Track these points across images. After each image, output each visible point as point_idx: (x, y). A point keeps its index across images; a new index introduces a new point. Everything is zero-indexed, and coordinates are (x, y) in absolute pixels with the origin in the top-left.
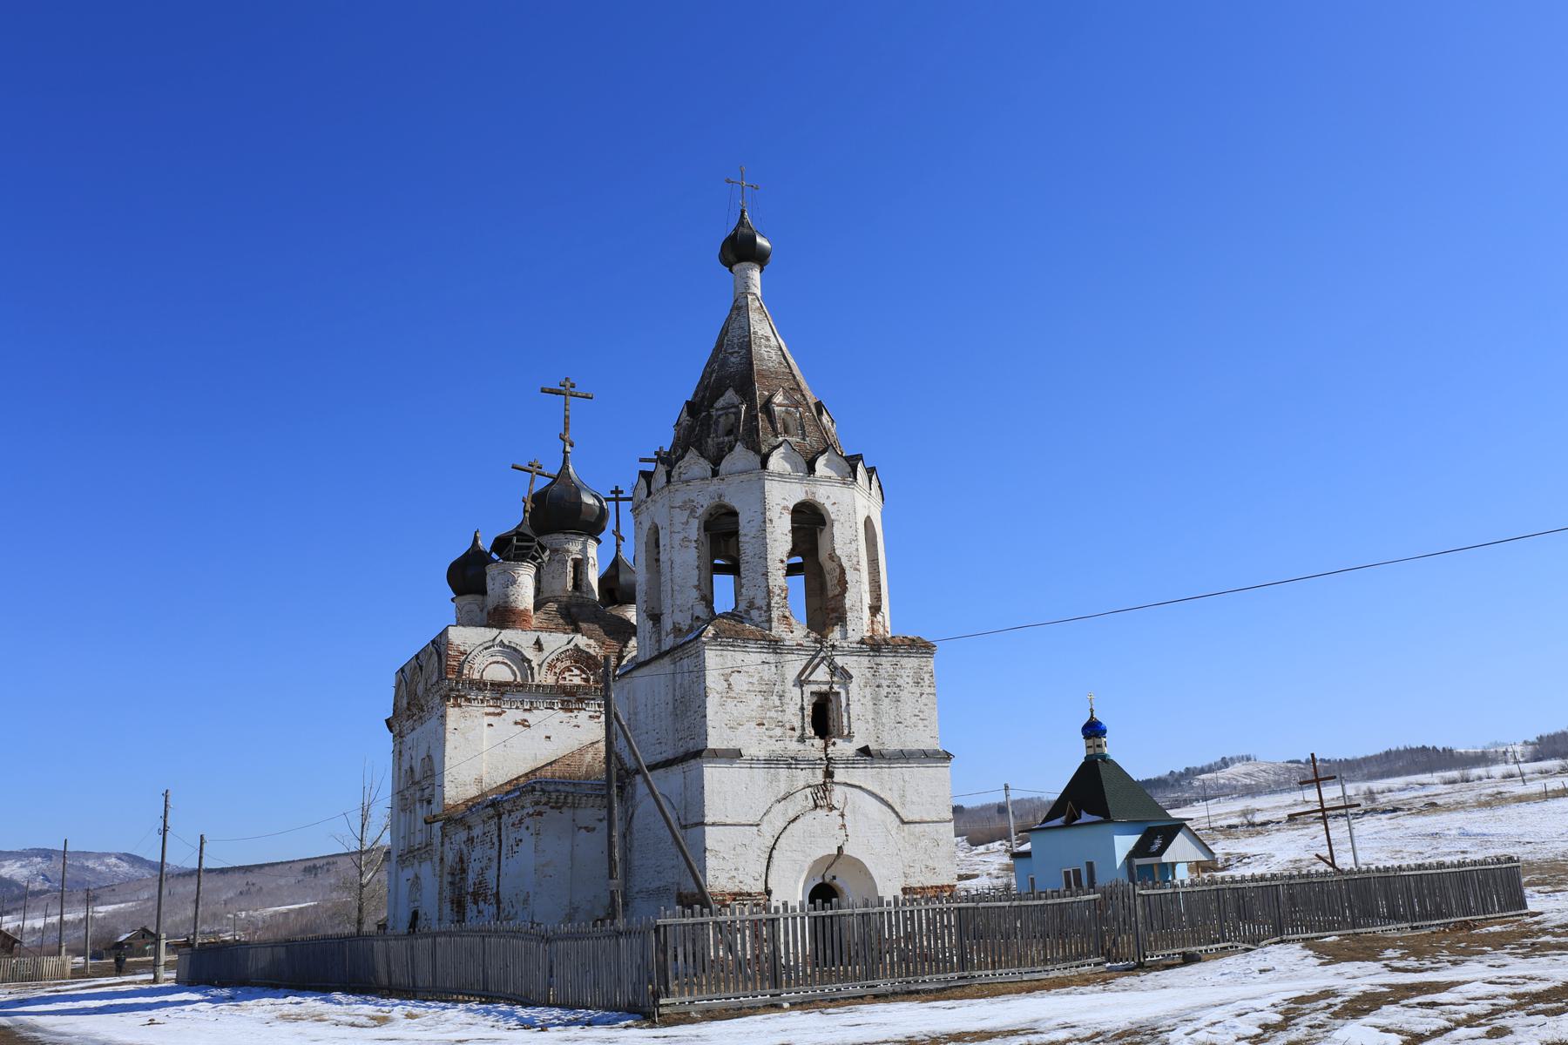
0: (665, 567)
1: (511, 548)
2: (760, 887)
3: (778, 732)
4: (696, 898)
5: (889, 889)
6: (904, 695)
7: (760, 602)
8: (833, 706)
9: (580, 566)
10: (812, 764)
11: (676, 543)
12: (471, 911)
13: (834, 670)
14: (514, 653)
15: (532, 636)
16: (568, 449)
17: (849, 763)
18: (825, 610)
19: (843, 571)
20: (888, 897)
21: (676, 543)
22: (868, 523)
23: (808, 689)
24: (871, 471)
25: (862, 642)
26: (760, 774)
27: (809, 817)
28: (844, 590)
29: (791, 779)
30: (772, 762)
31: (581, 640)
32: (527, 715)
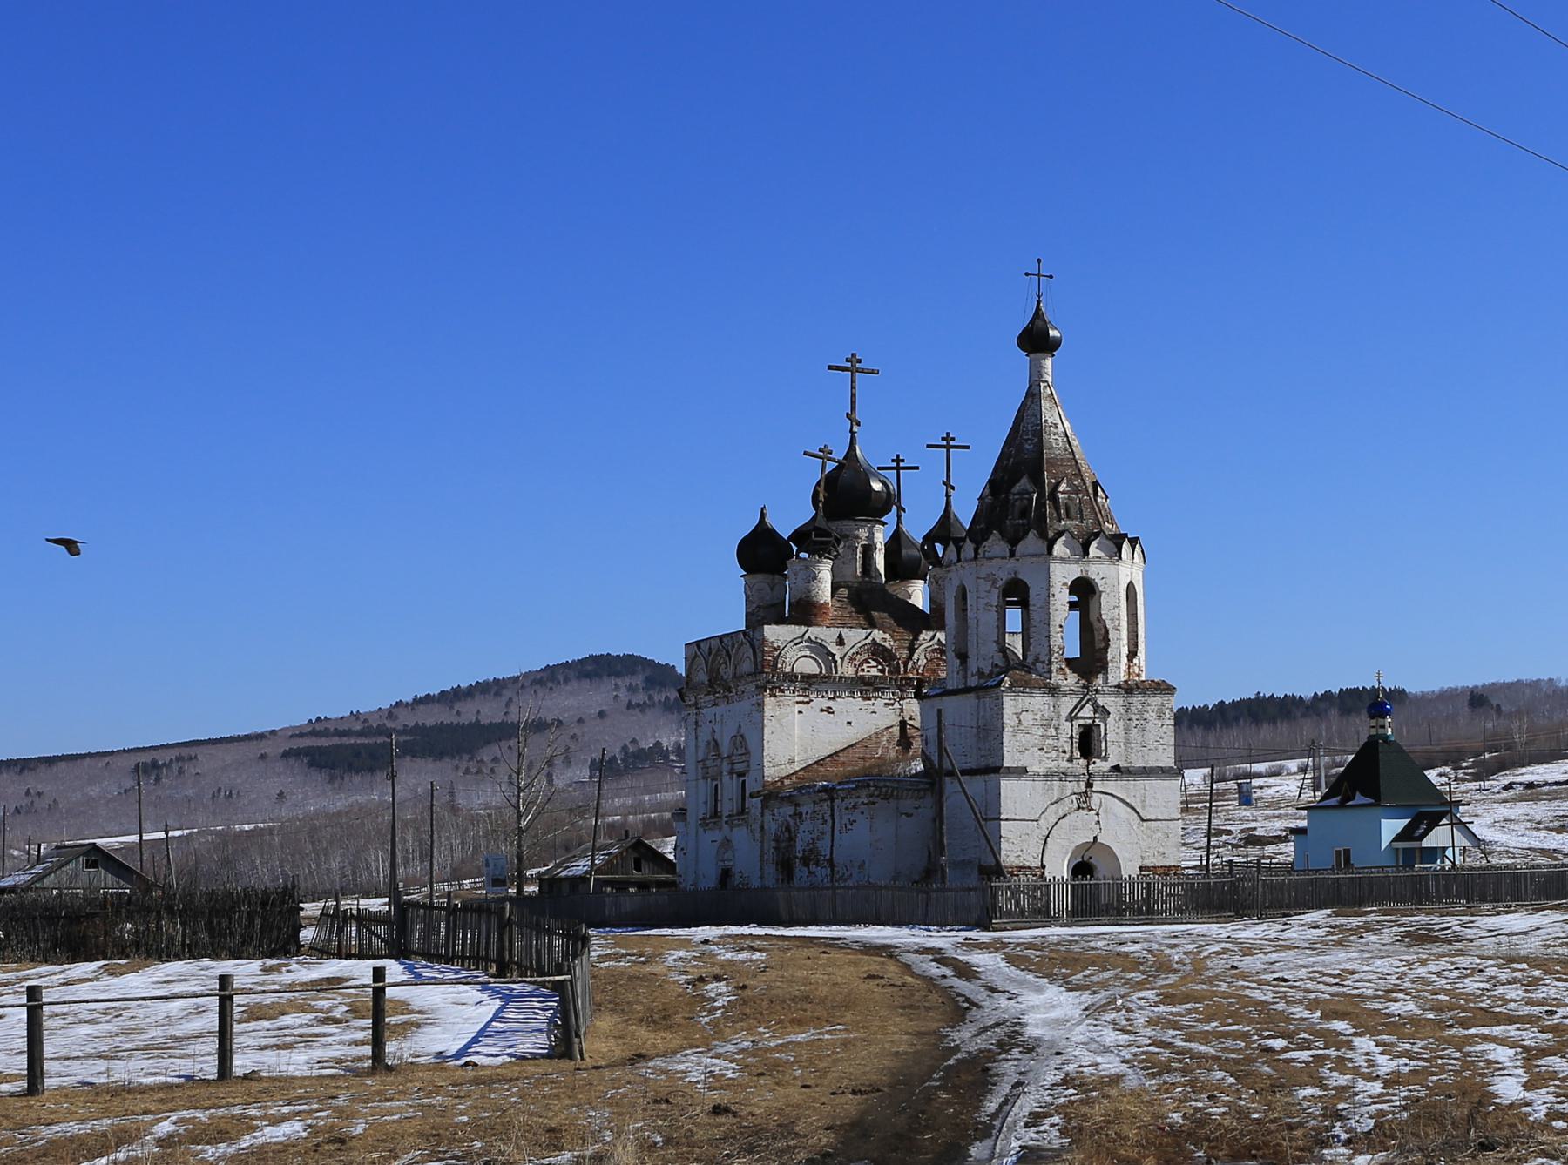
0: (972, 623)
1: (812, 539)
2: (1037, 863)
3: (1054, 754)
4: (997, 870)
5: (1129, 869)
6: (1149, 726)
7: (1044, 658)
8: (1095, 734)
9: (868, 550)
10: (1077, 777)
11: (981, 607)
12: (800, 872)
13: (1096, 708)
14: (819, 649)
15: (835, 632)
16: (855, 429)
17: (1104, 777)
18: (1091, 662)
19: (1107, 631)
20: (1125, 875)
21: (981, 607)
22: (1131, 588)
23: (1076, 723)
24: (1134, 542)
25: (1119, 686)
26: (1039, 784)
27: (1073, 815)
28: (1108, 646)
29: (1062, 788)
30: (1048, 776)
31: (877, 635)
32: (831, 703)
